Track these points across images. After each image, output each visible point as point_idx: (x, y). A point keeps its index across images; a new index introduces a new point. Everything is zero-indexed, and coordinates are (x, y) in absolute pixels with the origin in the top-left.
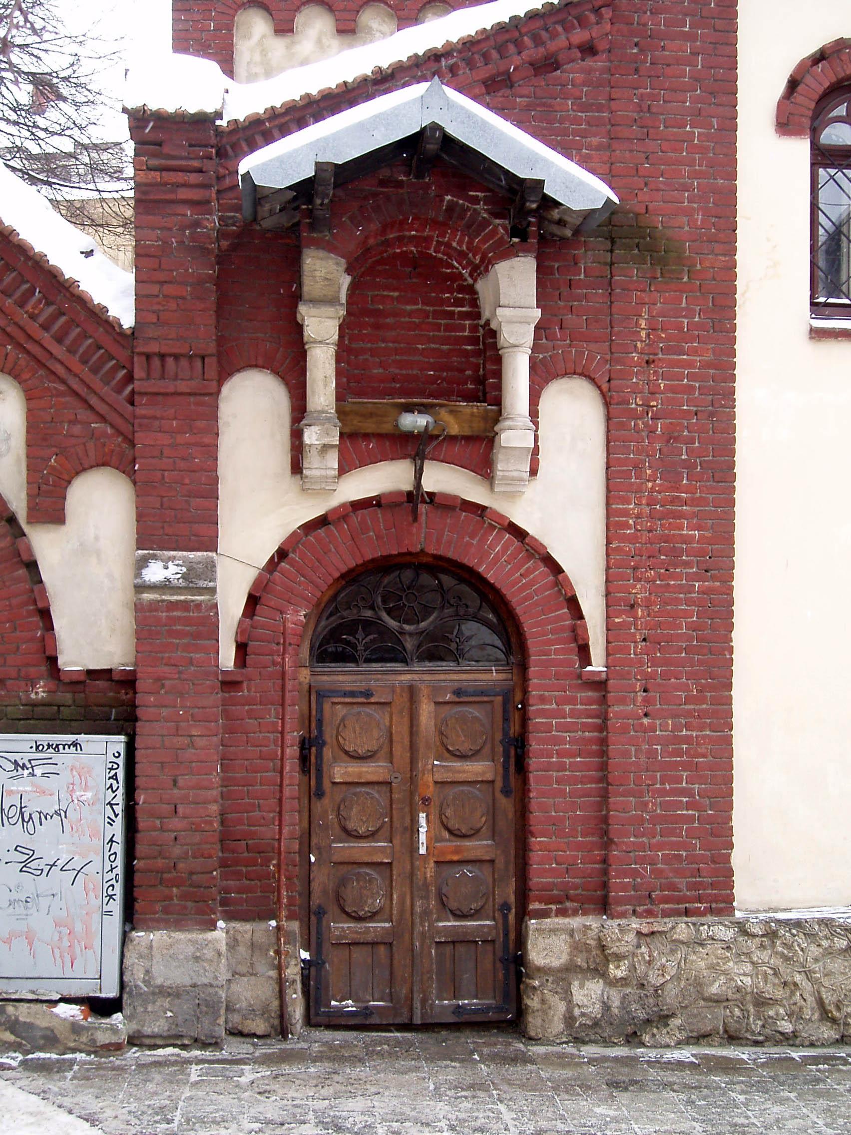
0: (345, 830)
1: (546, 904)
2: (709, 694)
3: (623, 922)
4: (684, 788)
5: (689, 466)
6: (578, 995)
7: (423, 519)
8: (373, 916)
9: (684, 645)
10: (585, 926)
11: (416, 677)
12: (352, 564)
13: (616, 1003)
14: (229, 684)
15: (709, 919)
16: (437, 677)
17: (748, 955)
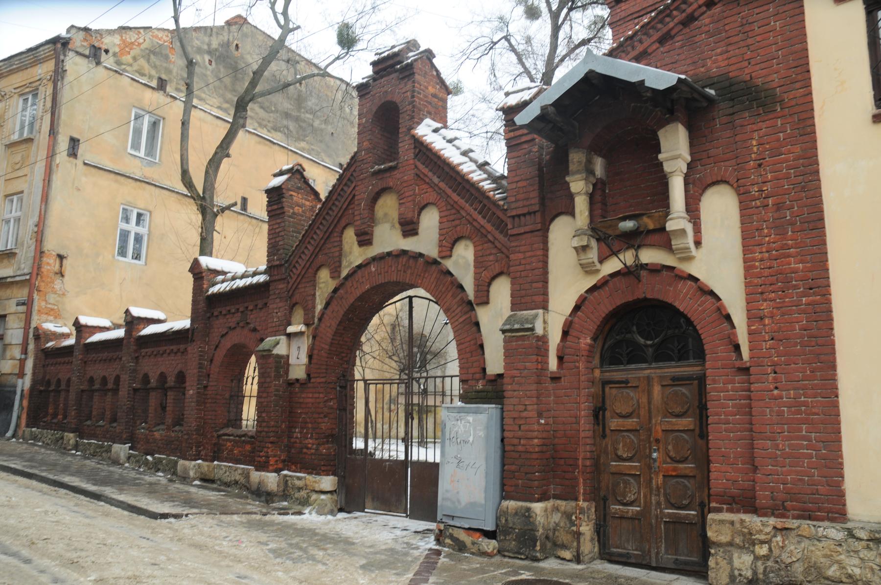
0: (616, 455)
1: (720, 504)
2: (818, 373)
3: (764, 519)
4: (804, 435)
5: (792, 223)
6: (737, 563)
7: (644, 280)
8: (631, 504)
9: (798, 341)
10: (741, 520)
11: (652, 371)
12: (611, 309)
13: (761, 569)
14: (555, 379)
15: (826, 523)
16: (663, 371)
17: (856, 552)
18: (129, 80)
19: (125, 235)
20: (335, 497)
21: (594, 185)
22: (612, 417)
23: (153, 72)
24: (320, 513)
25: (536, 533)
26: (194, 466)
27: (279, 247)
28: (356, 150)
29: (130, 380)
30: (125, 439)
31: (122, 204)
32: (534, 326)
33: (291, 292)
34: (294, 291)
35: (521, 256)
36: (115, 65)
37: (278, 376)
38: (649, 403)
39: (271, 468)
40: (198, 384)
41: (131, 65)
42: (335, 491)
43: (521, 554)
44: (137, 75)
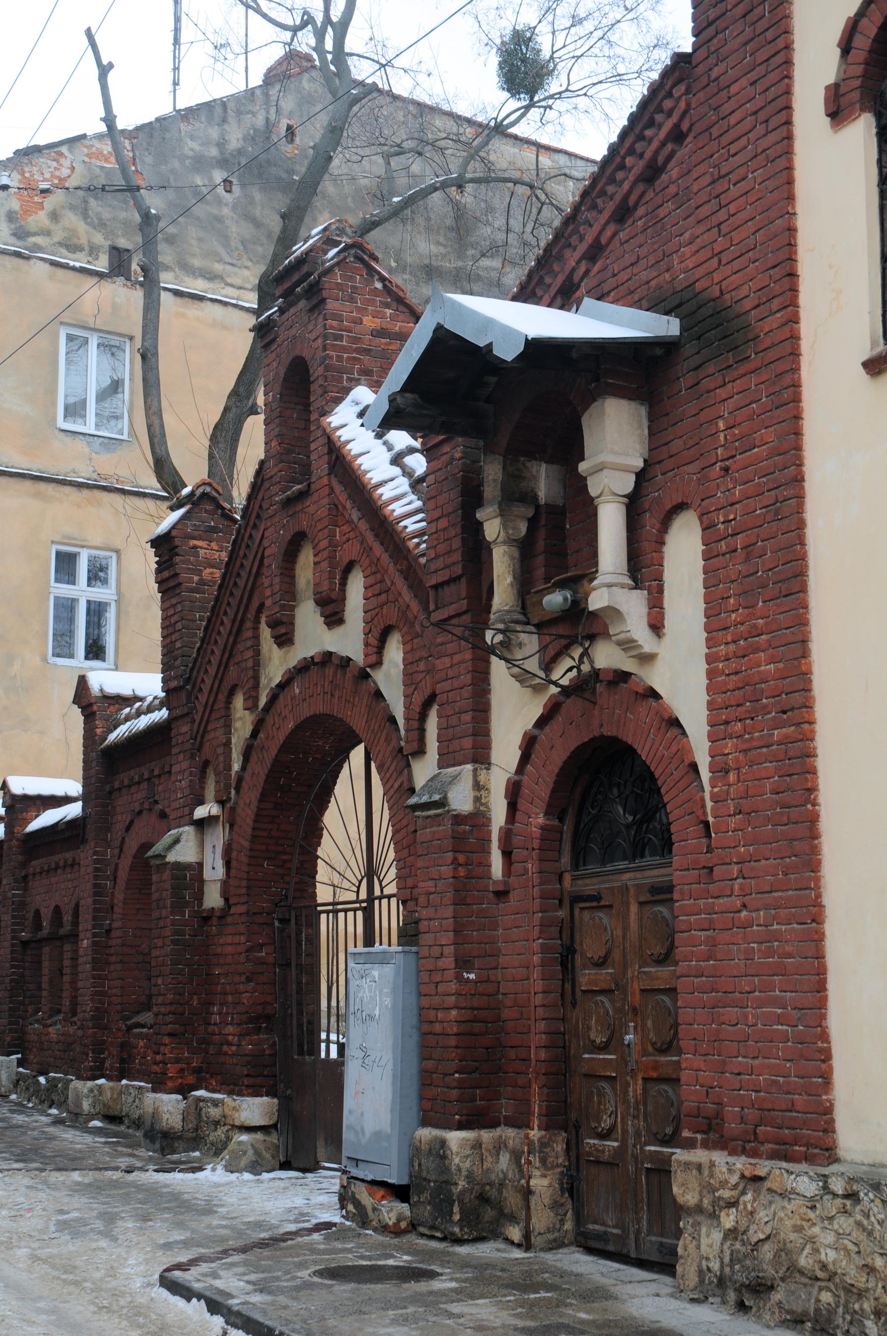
14: (502, 894)
18: (47, 266)
19: (66, 608)
20: (274, 1138)
21: (533, 522)
22: (585, 967)
23: (99, 239)
24: (230, 1169)
25: (453, 1188)
26: (91, 1091)
27: (176, 652)
28: (262, 456)
29: (14, 924)
30: (10, 1046)
31: (53, 542)
32: (445, 797)
33: (199, 738)
34: (203, 737)
35: (447, 660)
36: (13, 240)
37: (179, 905)
38: (624, 937)
39: (170, 1084)
40: (94, 928)
41: (48, 233)
42: (274, 1126)
43: (436, 1229)
44: (63, 251)
